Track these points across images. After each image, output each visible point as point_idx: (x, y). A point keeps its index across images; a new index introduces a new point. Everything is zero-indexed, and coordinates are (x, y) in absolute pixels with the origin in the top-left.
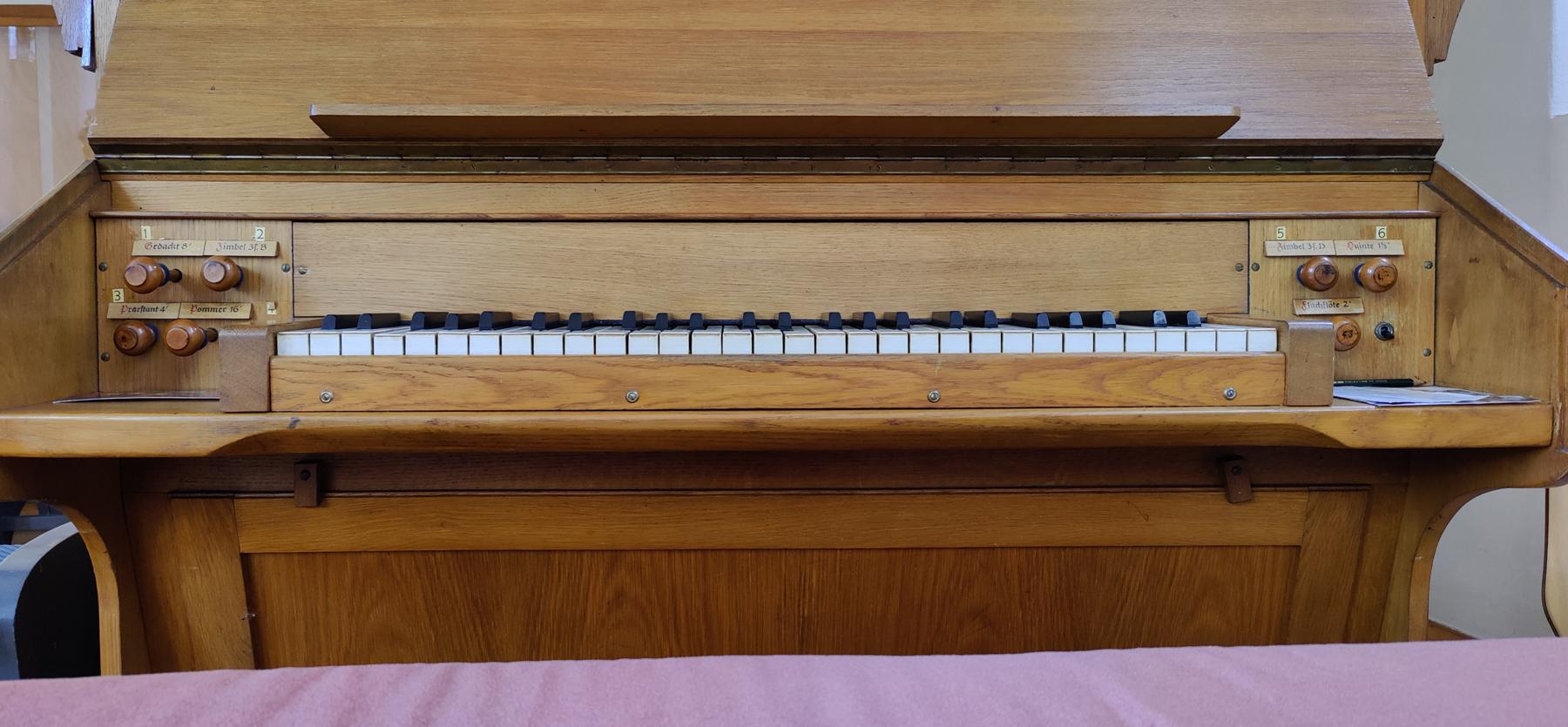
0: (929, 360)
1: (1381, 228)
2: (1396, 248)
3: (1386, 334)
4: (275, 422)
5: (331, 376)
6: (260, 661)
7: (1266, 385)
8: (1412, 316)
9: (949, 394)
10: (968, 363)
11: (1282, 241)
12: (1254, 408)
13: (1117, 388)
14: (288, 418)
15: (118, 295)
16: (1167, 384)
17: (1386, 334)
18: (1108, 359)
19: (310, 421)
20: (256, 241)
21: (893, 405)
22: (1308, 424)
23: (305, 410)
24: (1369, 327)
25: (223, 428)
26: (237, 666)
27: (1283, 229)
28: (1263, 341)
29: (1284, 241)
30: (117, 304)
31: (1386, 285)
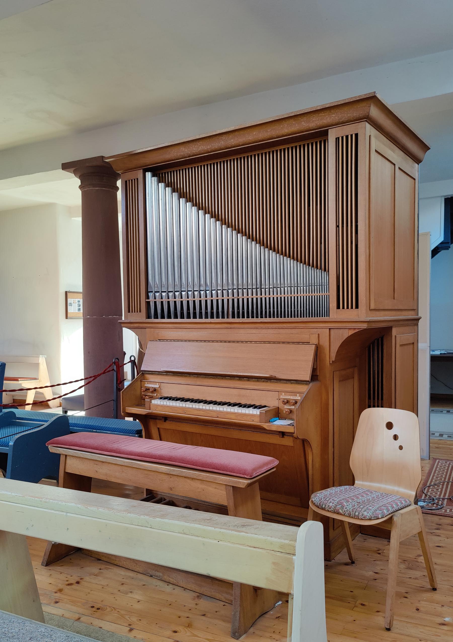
1: (298, 395)
12: (256, 422)
27: (283, 394)
29: (284, 396)
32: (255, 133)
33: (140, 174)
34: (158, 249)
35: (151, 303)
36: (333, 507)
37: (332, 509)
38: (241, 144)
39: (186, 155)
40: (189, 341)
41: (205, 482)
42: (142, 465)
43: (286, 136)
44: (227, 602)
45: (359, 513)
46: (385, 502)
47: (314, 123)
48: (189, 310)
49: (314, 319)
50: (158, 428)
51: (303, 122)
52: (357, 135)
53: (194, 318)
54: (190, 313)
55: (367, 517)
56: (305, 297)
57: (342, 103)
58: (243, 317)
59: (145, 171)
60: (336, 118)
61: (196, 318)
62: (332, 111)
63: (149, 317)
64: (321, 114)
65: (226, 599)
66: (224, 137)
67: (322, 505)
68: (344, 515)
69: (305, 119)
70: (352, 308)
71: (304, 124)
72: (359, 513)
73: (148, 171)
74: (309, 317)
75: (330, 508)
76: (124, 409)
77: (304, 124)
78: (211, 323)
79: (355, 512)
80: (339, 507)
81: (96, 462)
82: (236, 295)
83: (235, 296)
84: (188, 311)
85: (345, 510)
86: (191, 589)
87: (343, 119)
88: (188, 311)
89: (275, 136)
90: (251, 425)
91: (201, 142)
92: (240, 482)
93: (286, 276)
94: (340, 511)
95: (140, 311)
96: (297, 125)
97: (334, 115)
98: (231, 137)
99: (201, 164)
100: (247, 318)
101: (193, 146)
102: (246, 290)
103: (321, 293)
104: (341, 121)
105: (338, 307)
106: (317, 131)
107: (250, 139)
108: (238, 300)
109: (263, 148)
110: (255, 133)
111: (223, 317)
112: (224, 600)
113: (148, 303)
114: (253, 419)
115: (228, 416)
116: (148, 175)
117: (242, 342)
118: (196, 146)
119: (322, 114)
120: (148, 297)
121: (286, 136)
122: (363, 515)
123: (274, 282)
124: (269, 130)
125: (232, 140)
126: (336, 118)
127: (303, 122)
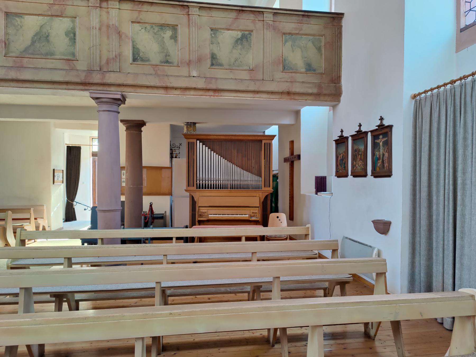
5: (211, 217)
12: (247, 218)
20: (206, 211)
21: (214, 218)
23: (210, 218)
31: (256, 213)
33: (195, 141)
47: (259, 138)
59: (197, 140)
113: (197, 184)
116: (198, 142)
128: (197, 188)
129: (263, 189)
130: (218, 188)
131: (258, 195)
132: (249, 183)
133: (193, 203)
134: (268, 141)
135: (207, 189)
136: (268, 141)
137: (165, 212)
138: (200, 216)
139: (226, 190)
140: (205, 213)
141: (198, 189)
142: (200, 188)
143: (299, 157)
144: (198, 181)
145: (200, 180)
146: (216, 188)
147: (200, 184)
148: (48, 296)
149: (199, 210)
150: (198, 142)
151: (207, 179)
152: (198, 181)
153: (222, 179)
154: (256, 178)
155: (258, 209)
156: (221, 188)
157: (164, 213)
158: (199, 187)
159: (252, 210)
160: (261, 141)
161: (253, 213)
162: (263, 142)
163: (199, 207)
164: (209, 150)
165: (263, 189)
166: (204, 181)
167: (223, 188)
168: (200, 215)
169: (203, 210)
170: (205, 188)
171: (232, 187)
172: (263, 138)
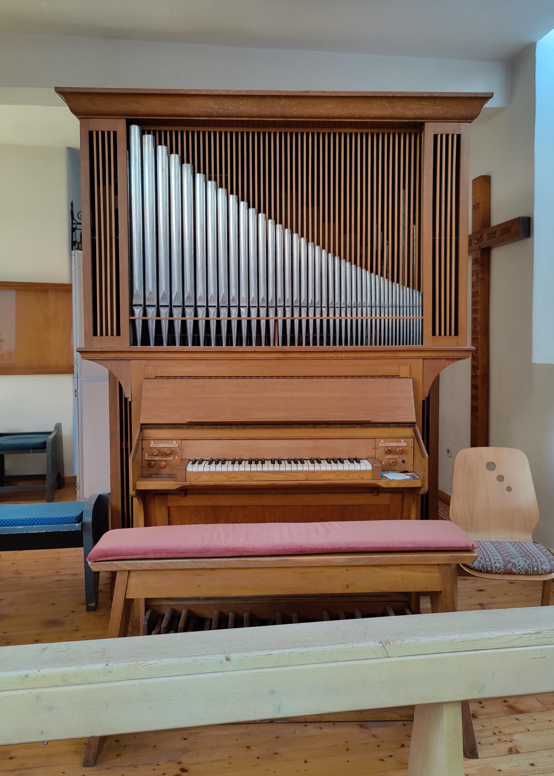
0: (306, 471)
1: (402, 440)
2: (405, 444)
3: (403, 462)
4: (187, 483)
5: (199, 472)
6: (169, 524)
7: (370, 476)
8: (409, 458)
9: (310, 478)
10: (314, 472)
11: (382, 443)
12: (368, 480)
13: (341, 477)
14: (189, 483)
15: (147, 455)
16: (351, 476)
17: (403, 462)
18: (340, 471)
19: (194, 483)
20: (174, 444)
21: (301, 480)
22: (376, 483)
23: (193, 481)
24: (400, 460)
25: (178, 485)
26: (164, 525)
27: (382, 441)
28: (369, 467)
29: (382, 443)
30: (147, 457)
31: (402, 452)
32: (330, 106)
33: (120, 125)
34: (225, 244)
35: (137, 321)
36: (502, 567)
37: (502, 570)
38: (306, 115)
39: (215, 113)
40: (359, 377)
41: (405, 567)
42: (300, 562)
43: (372, 118)
44: (404, 719)
45: (538, 568)
46: (515, 552)
47: (411, 111)
48: (198, 333)
49: (405, 347)
50: (168, 507)
51: (398, 107)
52: (459, 136)
53: (194, 344)
54: (210, 337)
55: (548, 571)
56: (405, 320)
57: (455, 96)
58: (328, 344)
59: (129, 123)
60: (441, 111)
61: (174, 344)
62: (438, 102)
63: (134, 343)
64: (423, 103)
65: (403, 716)
66: (283, 102)
67: (487, 568)
68: (519, 574)
69: (402, 103)
70: (450, 334)
71: (400, 110)
72: (538, 568)
73: (135, 124)
74: (396, 344)
75: (499, 569)
76: (135, 485)
77: (400, 110)
78: (335, 352)
79: (533, 568)
80: (509, 566)
81: (198, 572)
82: (288, 314)
83: (261, 316)
84: (196, 335)
85: (520, 567)
86: (345, 720)
87: (448, 115)
88: (196, 335)
89: (357, 116)
90: (209, 486)
91: (245, 101)
92: (466, 557)
93: (370, 294)
94: (514, 570)
95: (118, 334)
96: (389, 109)
97: (438, 108)
98: (293, 103)
99: (220, 130)
100: (333, 345)
101: (230, 104)
102: (204, 309)
103: (411, 316)
104: (445, 116)
105: (434, 334)
106: (389, 120)
107: (322, 112)
108: (346, 320)
109: (258, 126)
110: (330, 106)
111: (328, 344)
112: (399, 718)
113: (133, 323)
114: (363, 476)
115: (325, 477)
116: (135, 130)
117: (175, 377)
118: (234, 105)
119: (424, 103)
120: (132, 313)
121: (372, 118)
122: (542, 569)
123: (336, 301)
124: (351, 107)
125: (294, 109)
126: (441, 111)
127: (398, 107)
128: (134, 343)
129: (429, 342)
130: (229, 342)
131: (404, 371)
132: (366, 315)
133: (123, 410)
134: (450, 128)
135: (178, 347)
136: (450, 128)
137: (58, 427)
138: (150, 469)
139: (263, 347)
140: (172, 452)
141: (139, 347)
142: (145, 341)
143: (522, 228)
144: (138, 311)
145: (145, 307)
146: (219, 342)
147: (145, 323)
148: (242, 203)
149: (142, 439)
150: (135, 130)
151: (177, 302)
152: (138, 311)
153: (244, 303)
154: (403, 294)
155: (409, 432)
156: (239, 342)
157: (51, 429)
158: (143, 337)
159: (387, 440)
160: (415, 128)
161: (389, 451)
162: (430, 130)
163: (144, 426)
164: (187, 168)
165: (429, 342)
166: (164, 312)
167: (249, 343)
168: (150, 465)
169: (160, 442)
170: (172, 342)
171: (292, 337)
172: (427, 110)
